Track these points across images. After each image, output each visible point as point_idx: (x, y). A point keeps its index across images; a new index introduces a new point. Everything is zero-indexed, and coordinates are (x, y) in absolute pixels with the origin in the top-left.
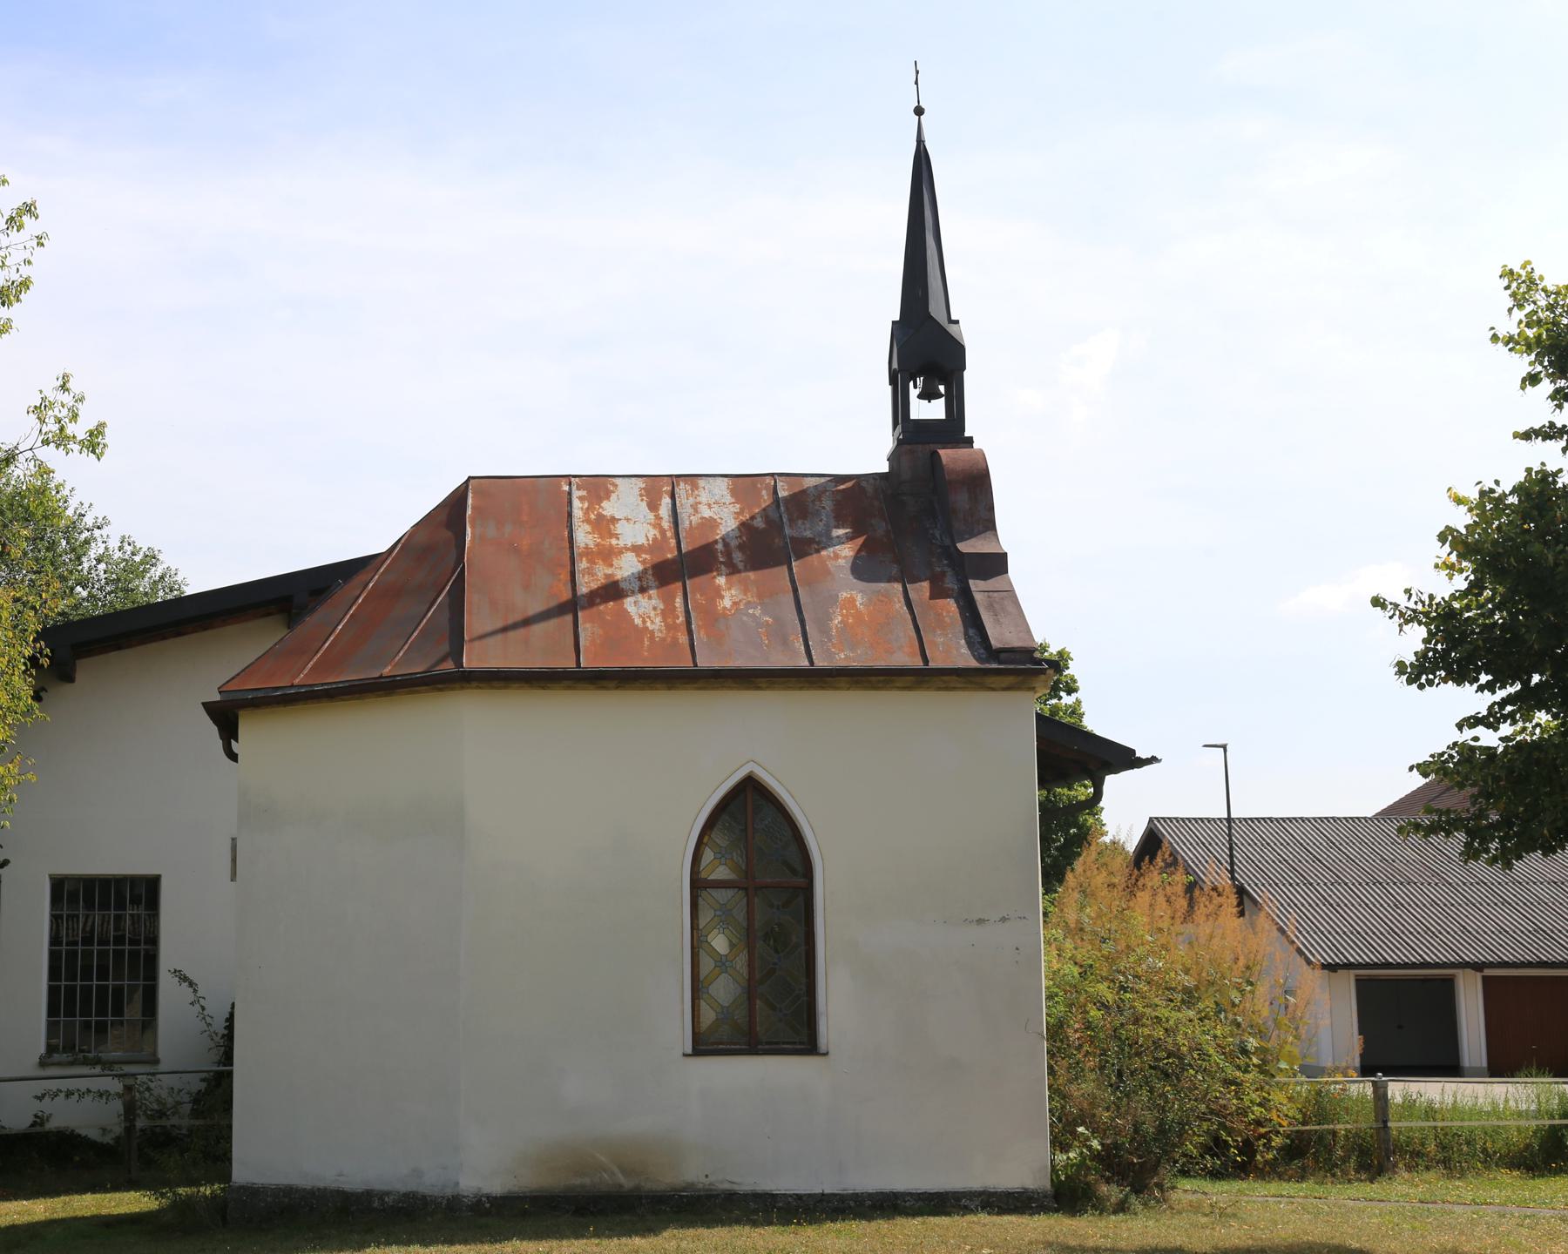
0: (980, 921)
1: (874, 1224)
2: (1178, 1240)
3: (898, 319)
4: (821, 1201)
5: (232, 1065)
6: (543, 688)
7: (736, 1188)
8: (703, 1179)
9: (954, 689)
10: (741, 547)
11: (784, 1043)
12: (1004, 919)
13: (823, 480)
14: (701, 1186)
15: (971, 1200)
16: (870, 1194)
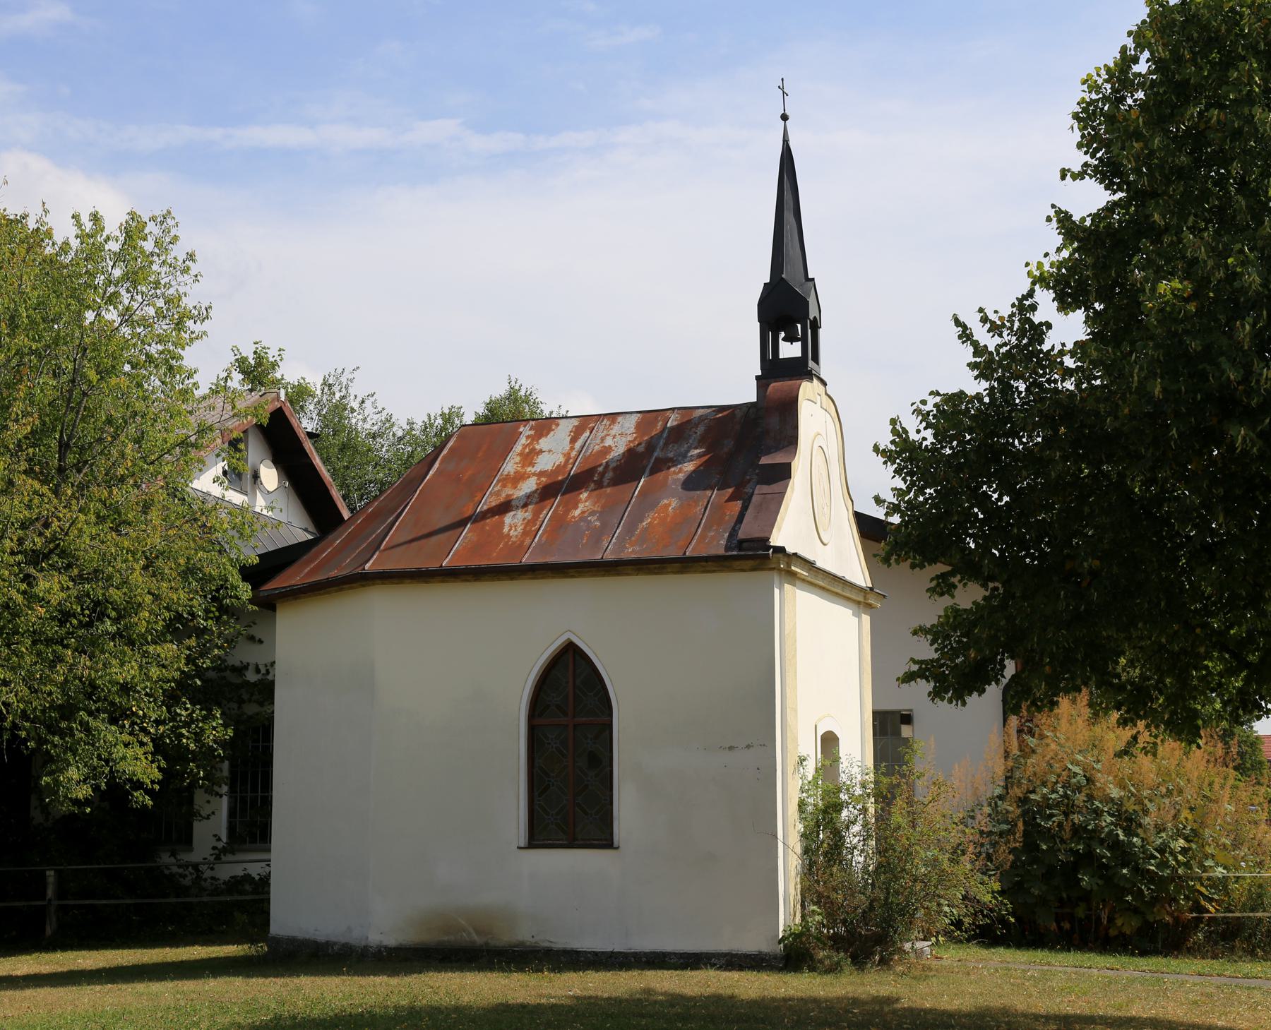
0: (731, 748)
1: (600, 974)
2: (1174, 1011)
3: (768, 281)
4: (611, 957)
5: (269, 850)
6: (426, 582)
7: (553, 945)
8: (531, 939)
9: (714, 571)
10: (615, 469)
11: (594, 840)
12: (748, 747)
13: (709, 411)
14: (528, 943)
15: (719, 959)
16: (645, 954)
